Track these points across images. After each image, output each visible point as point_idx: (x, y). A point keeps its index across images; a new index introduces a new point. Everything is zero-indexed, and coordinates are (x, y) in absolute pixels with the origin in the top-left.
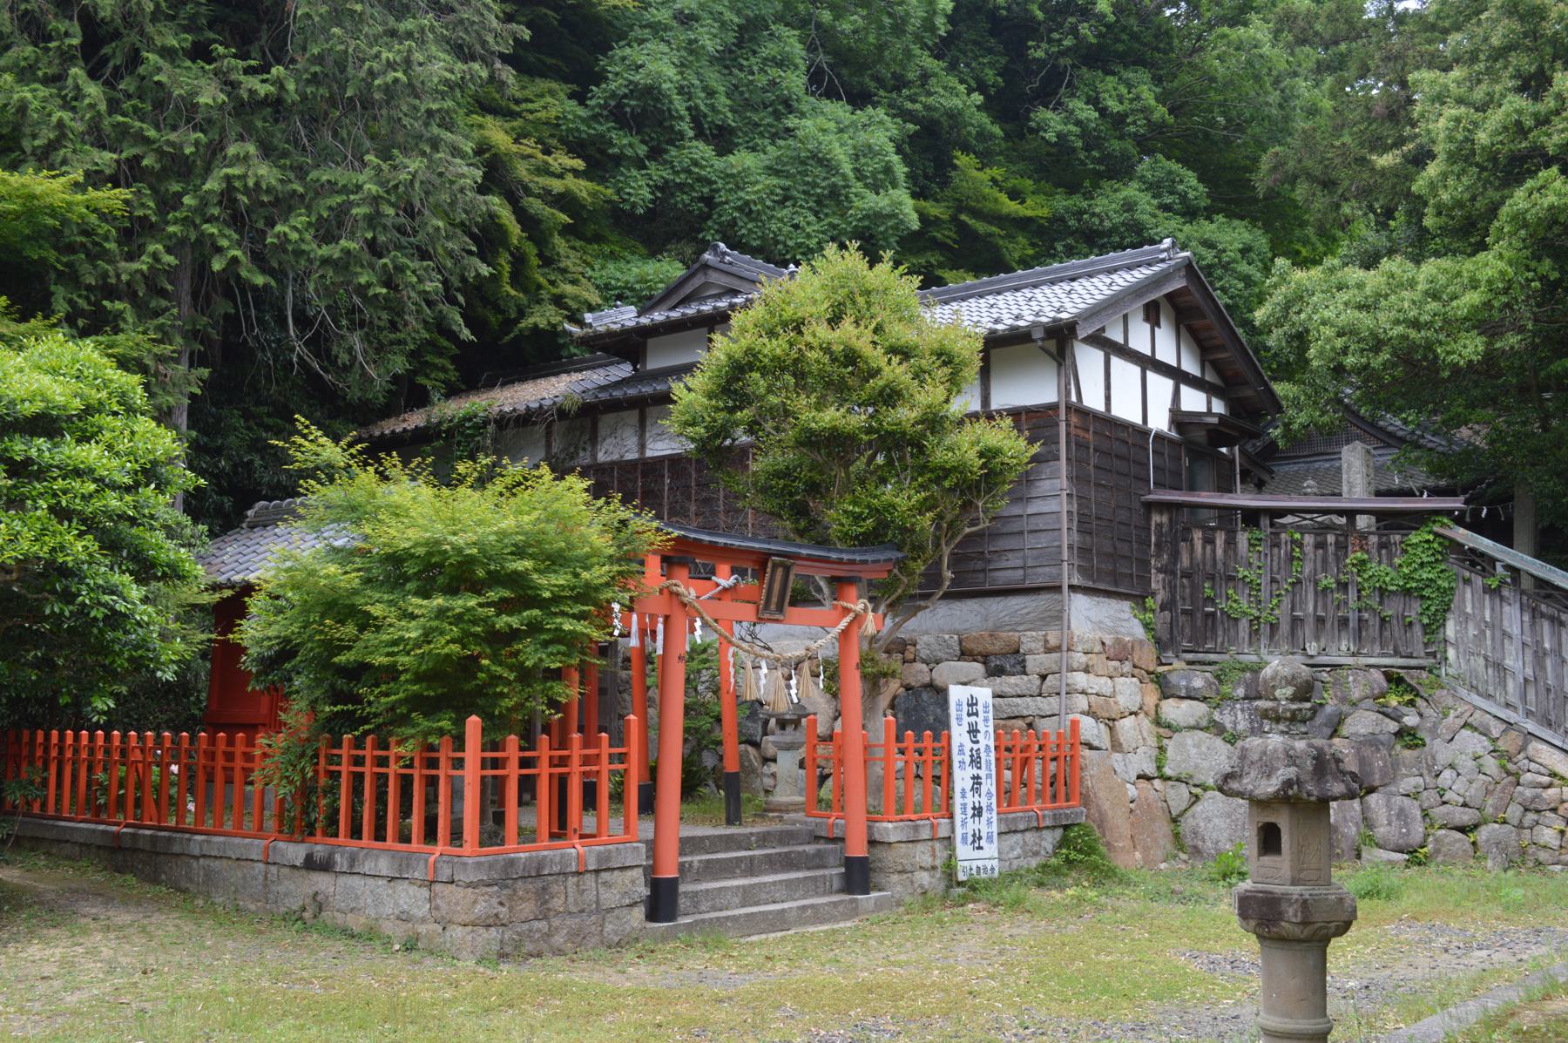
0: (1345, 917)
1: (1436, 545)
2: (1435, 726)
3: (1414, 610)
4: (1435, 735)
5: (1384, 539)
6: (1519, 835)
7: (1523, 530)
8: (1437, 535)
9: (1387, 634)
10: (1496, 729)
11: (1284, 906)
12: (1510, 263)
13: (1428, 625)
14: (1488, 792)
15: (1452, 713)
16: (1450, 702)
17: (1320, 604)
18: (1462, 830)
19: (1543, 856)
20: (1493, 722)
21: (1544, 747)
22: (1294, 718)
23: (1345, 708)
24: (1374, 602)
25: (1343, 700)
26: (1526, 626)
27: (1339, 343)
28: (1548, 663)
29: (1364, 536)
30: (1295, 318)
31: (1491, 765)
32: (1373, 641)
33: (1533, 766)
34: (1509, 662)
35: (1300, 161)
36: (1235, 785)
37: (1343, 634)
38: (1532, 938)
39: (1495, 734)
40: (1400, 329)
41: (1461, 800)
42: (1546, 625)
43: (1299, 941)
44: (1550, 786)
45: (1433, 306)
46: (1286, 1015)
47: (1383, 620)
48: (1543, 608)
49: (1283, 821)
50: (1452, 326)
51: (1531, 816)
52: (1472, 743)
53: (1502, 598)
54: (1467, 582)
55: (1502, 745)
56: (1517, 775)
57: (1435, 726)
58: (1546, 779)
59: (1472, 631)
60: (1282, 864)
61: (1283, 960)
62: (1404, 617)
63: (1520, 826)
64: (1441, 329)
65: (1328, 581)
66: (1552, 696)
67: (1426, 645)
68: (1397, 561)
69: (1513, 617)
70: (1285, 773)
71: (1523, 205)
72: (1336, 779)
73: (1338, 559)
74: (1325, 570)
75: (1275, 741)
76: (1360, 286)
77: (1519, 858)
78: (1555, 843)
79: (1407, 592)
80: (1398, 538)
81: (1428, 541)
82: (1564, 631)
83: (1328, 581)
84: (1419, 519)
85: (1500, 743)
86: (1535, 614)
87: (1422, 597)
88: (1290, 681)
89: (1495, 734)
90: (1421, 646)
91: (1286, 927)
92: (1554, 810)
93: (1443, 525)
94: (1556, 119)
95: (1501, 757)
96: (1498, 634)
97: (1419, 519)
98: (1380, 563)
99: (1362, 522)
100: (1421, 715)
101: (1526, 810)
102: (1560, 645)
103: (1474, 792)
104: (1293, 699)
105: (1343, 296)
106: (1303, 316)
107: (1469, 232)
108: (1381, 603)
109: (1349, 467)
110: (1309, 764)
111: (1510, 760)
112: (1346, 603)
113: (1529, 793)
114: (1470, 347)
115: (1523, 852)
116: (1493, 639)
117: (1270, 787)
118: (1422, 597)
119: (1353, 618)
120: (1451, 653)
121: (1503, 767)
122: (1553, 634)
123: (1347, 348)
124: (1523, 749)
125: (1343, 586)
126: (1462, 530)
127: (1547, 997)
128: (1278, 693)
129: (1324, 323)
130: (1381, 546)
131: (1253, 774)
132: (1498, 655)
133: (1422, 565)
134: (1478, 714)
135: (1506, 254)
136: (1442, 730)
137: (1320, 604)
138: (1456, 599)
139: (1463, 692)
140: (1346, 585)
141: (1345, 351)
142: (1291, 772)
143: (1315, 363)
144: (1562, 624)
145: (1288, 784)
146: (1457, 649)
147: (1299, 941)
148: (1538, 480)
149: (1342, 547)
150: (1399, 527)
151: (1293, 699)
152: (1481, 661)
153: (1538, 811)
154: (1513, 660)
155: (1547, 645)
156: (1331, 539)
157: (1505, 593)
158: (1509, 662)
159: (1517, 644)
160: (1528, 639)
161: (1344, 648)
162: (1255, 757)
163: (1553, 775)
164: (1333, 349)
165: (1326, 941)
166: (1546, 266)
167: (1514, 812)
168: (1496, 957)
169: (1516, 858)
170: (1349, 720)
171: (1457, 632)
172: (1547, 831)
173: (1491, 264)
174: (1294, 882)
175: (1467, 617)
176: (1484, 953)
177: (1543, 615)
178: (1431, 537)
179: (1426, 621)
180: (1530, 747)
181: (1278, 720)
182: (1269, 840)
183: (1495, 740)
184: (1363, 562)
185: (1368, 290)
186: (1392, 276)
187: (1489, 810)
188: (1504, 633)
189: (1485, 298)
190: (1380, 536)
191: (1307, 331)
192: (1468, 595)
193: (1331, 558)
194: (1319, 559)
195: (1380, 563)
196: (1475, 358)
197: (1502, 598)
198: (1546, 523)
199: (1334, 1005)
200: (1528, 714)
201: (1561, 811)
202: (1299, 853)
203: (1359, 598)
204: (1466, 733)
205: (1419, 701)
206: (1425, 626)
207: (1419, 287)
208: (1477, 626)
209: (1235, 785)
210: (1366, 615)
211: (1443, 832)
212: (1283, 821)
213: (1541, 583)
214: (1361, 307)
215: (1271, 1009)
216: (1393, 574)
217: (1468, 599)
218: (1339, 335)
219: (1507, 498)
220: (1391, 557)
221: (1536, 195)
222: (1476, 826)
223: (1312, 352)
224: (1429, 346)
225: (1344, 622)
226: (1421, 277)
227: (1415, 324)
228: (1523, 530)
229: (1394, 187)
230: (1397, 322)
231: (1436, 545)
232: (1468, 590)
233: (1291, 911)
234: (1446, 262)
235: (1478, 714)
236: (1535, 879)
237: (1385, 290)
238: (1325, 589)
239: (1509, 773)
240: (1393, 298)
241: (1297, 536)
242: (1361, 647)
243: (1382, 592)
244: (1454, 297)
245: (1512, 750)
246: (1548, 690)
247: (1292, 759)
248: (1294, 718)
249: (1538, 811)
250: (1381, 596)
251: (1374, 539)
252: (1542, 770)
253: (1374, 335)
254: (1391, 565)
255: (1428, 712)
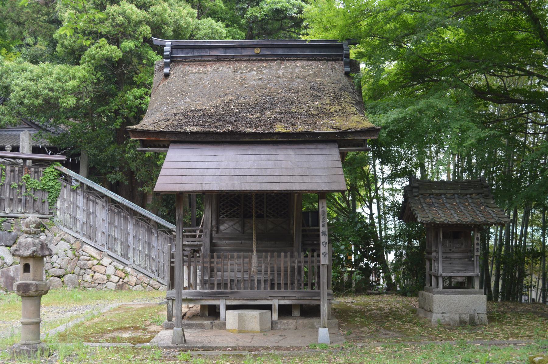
0: (47, 289)
1: (55, 173)
2: (51, 239)
3: (46, 196)
4: (51, 243)
5: (36, 170)
6: (78, 278)
7: (83, 168)
8: (56, 169)
9: (35, 205)
10: (72, 240)
11: (31, 287)
12: (88, 72)
13: (51, 202)
14: (68, 263)
15: (57, 235)
16: (57, 231)
17: (11, 193)
18: (59, 277)
19: (86, 285)
20: (71, 238)
21: (88, 246)
22: (35, 233)
23: (19, 233)
24: (31, 194)
25: (19, 230)
26: (85, 203)
27: (22, 93)
28: (91, 217)
29: (29, 168)
30: (5, 80)
31: (70, 253)
32: (30, 208)
33: (84, 253)
34: (78, 216)
35: (8, 13)
36: (17, 253)
37: (19, 205)
38: (85, 308)
39: (72, 242)
40: (46, 91)
41: (59, 266)
42: (91, 203)
43: (34, 296)
44: (89, 260)
45: (59, 84)
46: (30, 318)
47: (34, 200)
48: (91, 197)
49: (31, 263)
50: (65, 91)
51: (83, 271)
52: (64, 245)
53: (77, 193)
54: (65, 187)
55: (74, 246)
56: (79, 257)
57: (51, 239)
58: (88, 258)
59: (66, 205)
60: (30, 275)
61: (29, 303)
62: (42, 199)
63: (79, 275)
64: (61, 93)
65: (15, 185)
66: (92, 228)
67: (49, 210)
68: (41, 178)
69: (80, 200)
70: (33, 249)
71: (94, 52)
72: (46, 250)
73: (19, 176)
74: (14, 180)
75: (30, 240)
76: (31, 72)
77: (79, 285)
78: (90, 280)
79: (44, 190)
80: (41, 169)
81: (52, 171)
82: (97, 206)
83: (15, 185)
84: (48, 163)
85: (73, 245)
86: (88, 199)
87: (49, 192)
88: (34, 223)
89: (72, 242)
90: (48, 210)
91: (31, 293)
92: (90, 268)
93: (58, 166)
94: (106, 22)
95: (73, 250)
96: (75, 206)
97: (48, 163)
98: (34, 178)
99: (29, 163)
100: (46, 236)
101: (81, 269)
102: (95, 211)
103: (64, 263)
104: (35, 228)
105: (25, 74)
106: (8, 80)
107: (74, 56)
108: (34, 194)
109: (23, 140)
110: (39, 246)
111: (76, 251)
112: (21, 193)
113: (82, 263)
114: (71, 101)
115: (79, 284)
116: (73, 208)
117: (28, 253)
118: (49, 192)
119: (23, 199)
120: (58, 213)
121: (74, 254)
122: (93, 206)
123: (25, 95)
124: (81, 247)
125: (20, 187)
126: (64, 168)
127: (92, 319)
128: (31, 226)
129: (16, 85)
130: (36, 172)
131: (23, 249)
132: (75, 214)
133: (50, 180)
134: (66, 235)
135: (87, 69)
136: (54, 241)
137: (11, 193)
138: (61, 193)
139: (61, 227)
140: (21, 186)
141: (24, 97)
142: (35, 249)
143: (12, 101)
144: (96, 203)
145: (34, 252)
146: (60, 211)
147: (34, 296)
148: (90, 149)
149: (21, 172)
150: (41, 165)
151: (35, 228)
152: (69, 216)
153: (85, 269)
154: (80, 216)
155: (91, 211)
156: (17, 169)
157: (78, 191)
158: (78, 216)
159: (81, 210)
160: (85, 208)
161: (19, 210)
162: (24, 244)
163: (91, 256)
164: (19, 95)
165: (41, 296)
166: (99, 75)
167: (77, 270)
168: (75, 313)
169: (77, 286)
170: (20, 238)
171: (61, 205)
172: (88, 276)
173: (81, 71)
174: (33, 280)
175: (64, 200)
176: (70, 313)
177: (90, 200)
178: (53, 170)
179: (50, 201)
180: (83, 247)
181: (30, 234)
182: (27, 268)
183: (72, 244)
184: (28, 178)
185: (34, 74)
186: (44, 69)
187: (69, 269)
188: (77, 206)
189: (79, 84)
190: (35, 168)
191: (9, 86)
192: (65, 192)
193: (16, 176)
194: (12, 176)
195: (34, 178)
196: (72, 105)
197: (77, 193)
198: (92, 165)
199: (42, 317)
200: (84, 235)
201: (92, 269)
202: (35, 271)
203: (26, 192)
204: (62, 242)
205: (46, 231)
206: (49, 203)
207: (54, 76)
208: (68, 203)
209: (17, 253)
210: (28, 198)
211: (52, 278)
212: (31, 263)
213: (89, 187)
214: (31, 80)
215: (24, 317)
216: (39, 183)
217: (65, 193)
218: (22, 90)
219: (79, 155)
220: (38, 177)
221: (98, 49)
222: (64, 275)
223: (11, 96)
224: (57, 99)
225: (20, 200)
226: (55, 72)
227: (51, 90)
228: (83, 168)
229: (46, 32)
230: (45, 88)
231: (55, 173)
232: (65, 190)
233: (33, 288)
234: (64, 67)
235: (66, 235)
236: (83, 292)
237: (41, 74)
238: (14, 188)
239: (76, 256)
240: (44, 79)
241: (4, 167)
242: (26, 210)
243: (35, 189)
244: (66, 81)
245: (77, 248)
246: (91, 226)
247: (34, 245)
248: (35, 233)
249: (85, 269)
250: (34, 191)
251: (33, 169)
252: (87, 255)
253: (36, 92)
254: (38, 179)
255: (49, 234)
